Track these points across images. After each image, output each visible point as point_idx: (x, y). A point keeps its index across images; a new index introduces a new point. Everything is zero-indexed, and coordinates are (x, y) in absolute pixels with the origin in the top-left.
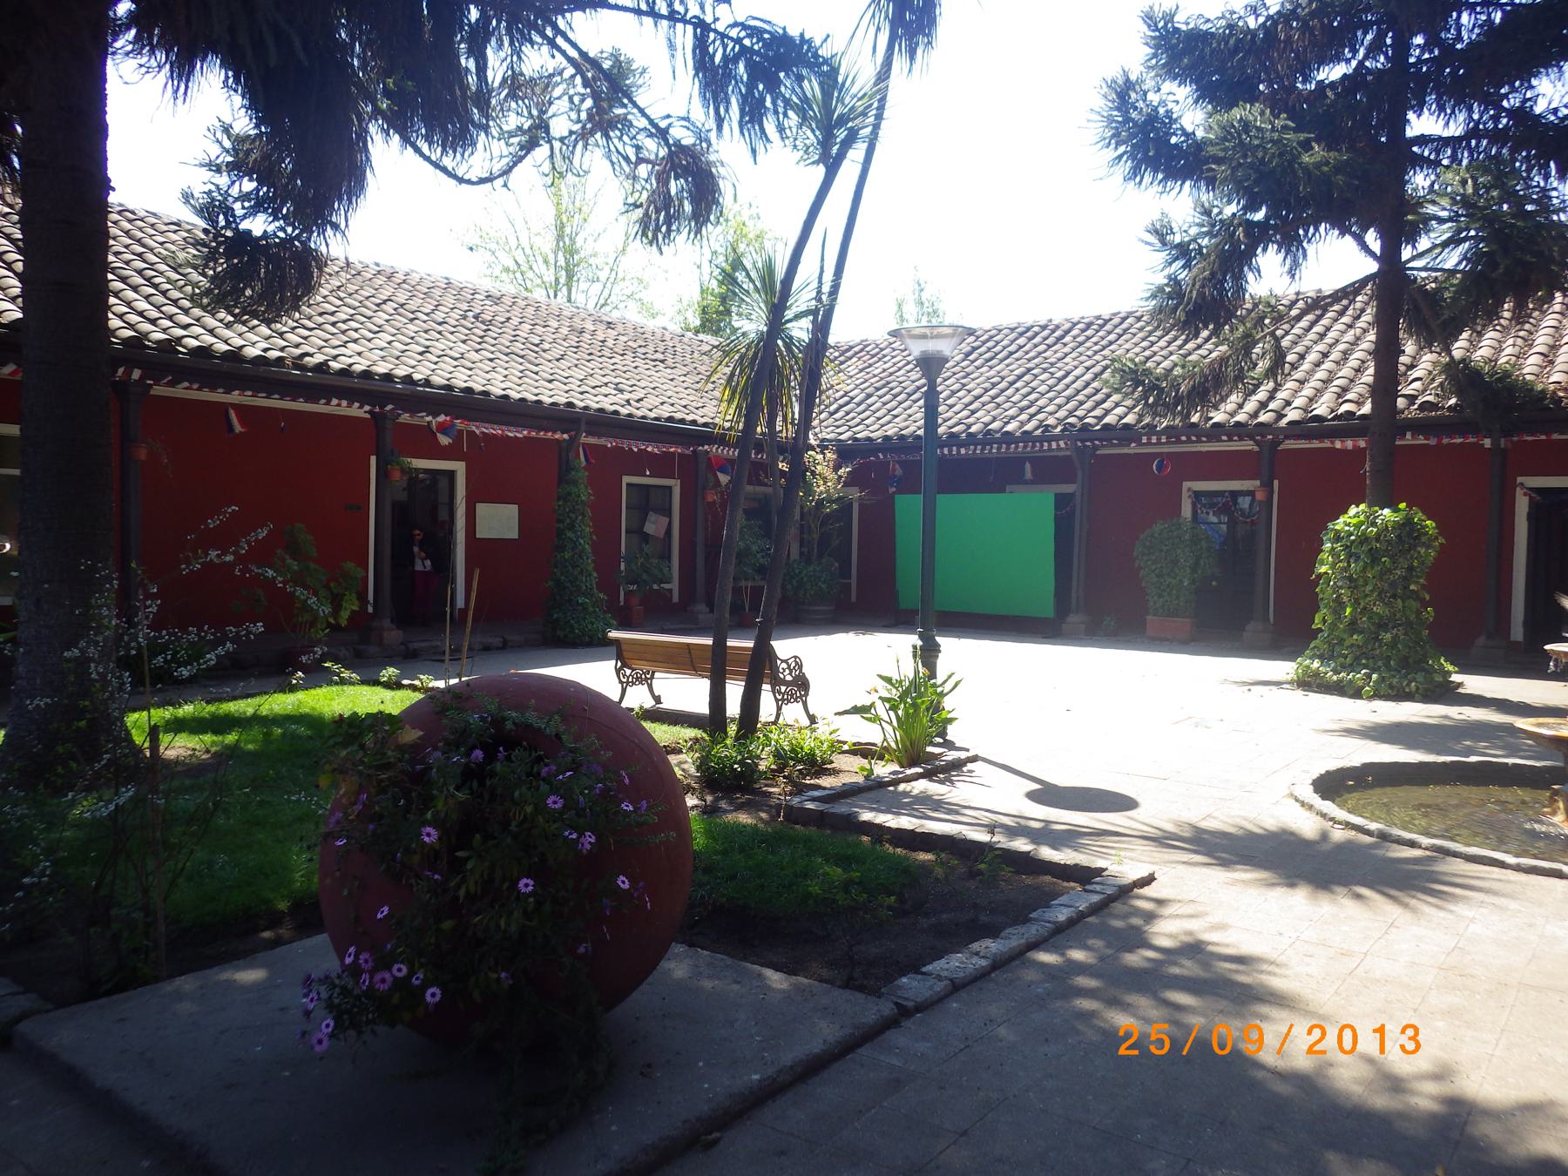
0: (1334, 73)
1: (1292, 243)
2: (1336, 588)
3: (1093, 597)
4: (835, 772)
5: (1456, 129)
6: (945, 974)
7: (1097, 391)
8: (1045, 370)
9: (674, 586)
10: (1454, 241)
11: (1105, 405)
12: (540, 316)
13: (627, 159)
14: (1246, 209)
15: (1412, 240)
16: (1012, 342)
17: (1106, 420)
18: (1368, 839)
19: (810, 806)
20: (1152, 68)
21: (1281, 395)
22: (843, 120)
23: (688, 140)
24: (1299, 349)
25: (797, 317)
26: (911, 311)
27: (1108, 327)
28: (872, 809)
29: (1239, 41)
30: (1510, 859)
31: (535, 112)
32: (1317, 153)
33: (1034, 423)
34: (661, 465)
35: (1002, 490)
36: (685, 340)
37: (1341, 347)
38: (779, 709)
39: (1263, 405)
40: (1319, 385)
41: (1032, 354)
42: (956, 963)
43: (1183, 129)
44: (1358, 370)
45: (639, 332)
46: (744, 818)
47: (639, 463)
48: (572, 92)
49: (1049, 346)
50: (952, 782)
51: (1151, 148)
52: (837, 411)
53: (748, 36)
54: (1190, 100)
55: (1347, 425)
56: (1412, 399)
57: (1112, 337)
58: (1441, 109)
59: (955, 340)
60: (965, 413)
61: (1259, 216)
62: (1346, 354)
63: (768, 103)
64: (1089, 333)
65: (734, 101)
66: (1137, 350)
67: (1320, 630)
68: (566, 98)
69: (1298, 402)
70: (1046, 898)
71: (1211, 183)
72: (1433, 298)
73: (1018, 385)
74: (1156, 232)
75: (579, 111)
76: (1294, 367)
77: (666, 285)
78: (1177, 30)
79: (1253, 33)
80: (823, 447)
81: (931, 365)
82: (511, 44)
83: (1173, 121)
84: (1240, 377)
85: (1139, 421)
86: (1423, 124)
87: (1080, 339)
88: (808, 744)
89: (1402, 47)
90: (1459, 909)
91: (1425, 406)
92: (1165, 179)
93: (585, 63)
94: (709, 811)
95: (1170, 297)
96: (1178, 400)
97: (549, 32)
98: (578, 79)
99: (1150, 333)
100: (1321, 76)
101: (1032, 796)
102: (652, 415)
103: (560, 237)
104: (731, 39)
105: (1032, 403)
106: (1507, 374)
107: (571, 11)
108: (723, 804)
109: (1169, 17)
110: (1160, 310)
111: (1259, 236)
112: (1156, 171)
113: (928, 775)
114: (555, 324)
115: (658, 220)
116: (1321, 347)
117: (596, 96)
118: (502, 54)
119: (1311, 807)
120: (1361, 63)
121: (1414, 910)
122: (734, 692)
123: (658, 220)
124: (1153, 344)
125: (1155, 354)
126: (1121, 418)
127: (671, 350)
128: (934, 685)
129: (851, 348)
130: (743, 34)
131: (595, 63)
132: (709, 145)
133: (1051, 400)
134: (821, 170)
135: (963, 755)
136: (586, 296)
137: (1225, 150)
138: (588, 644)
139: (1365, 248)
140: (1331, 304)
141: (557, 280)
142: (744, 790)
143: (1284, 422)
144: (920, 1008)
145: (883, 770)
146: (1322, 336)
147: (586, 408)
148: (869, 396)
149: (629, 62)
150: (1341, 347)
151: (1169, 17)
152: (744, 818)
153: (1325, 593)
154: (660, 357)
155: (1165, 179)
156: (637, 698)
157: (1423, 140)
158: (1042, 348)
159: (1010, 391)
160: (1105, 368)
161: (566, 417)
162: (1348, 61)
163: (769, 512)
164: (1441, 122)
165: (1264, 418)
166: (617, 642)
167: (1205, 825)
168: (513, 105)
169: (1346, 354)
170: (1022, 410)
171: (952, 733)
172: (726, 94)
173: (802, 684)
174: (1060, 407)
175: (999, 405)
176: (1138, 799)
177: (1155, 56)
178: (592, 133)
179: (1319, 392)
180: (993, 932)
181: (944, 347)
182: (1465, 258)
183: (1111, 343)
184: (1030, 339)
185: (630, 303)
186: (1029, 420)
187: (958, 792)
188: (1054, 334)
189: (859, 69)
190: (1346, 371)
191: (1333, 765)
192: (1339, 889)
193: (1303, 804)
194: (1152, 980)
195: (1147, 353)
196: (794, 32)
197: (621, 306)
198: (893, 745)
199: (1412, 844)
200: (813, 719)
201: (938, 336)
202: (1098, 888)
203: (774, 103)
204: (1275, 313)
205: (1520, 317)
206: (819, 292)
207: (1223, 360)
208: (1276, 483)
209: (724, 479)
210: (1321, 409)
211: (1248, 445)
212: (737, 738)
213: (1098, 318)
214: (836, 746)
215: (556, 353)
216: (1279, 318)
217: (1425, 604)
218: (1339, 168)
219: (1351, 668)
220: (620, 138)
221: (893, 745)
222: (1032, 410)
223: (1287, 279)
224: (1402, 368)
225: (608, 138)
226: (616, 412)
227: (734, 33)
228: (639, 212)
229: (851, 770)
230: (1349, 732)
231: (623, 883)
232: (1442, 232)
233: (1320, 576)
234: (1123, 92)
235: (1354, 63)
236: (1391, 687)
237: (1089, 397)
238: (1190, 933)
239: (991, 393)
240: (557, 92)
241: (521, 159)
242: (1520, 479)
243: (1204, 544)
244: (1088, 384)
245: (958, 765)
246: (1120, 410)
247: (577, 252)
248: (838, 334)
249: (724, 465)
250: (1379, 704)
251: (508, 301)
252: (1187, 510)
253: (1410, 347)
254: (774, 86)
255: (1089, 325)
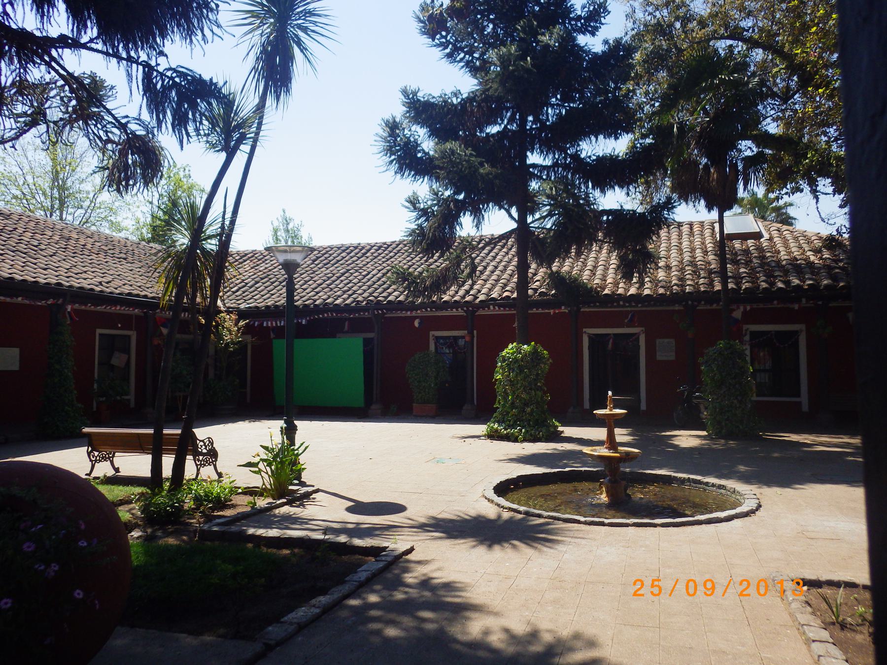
0: (494, 129)
1: (477, 214)
2: (505, 386)
3: (387, 396)
4: (234, 506)
5: (548, 162)
6: (295, 620)
7: (385, 283)
8: (357, 271)
9: (131, 397)
10: (550, 214)
11: (389, 291)
12: (39, 228)
13: (100, 138)
14: (455, 193)
15: (532, 213)
16: (339, 255)
17: (389, 299)
18: (520, 516)
19: (215, 529)
20: (407, 118)
21: (476, 287)
22: (239, 126)
23: (141, 132)
24: (484, 264)
25: (210, 237)
26: (281, 234)
27: (390, 249)
28: (255, 527)
29: (449, 109)
30: (582, 519)
31: (35, 104)
32: (486, 169)
33: (351, 300)
34: (126, 321)
35: (334, 336)
36: (141, 246)
37: (503, 264)
38: (198, 470)
39: (467, 292)
40: (493, 282)
41: (349, 262)
42: (302, 613)
43: (423, 150)
44: (511, 276)
45: (109, 240)
46: (171, 541)
47: (109, 320)
48: (62, 95)
49: (359, 258)
50: (304, 506)
51: (407, 159)
52: (237, 291)
53: (177, 76)
54: (426, 136)
55: (505, 302)
56: (535, 290)
57: (392, 254)
58: (542, 152)
59: (303, 255)
60: (313, 293)
61: (461, 197)
62: (506, 267)
63: (190, 116)
64: (380, 251)
65: (169, 112)
66: (405, 261)
67: (498, 408)
68: (58, 98)
69: (484, 291)
70: (354, 568)
71: (438, 179)
72: (542, 242)
73: (342, 278)
74: (410, 202)
75: (67, 107)
76: (482, 273)
77: (132, 213)
78: (419, 100)
79: (455, 106)
80: (229, 311)
81: (290, 267)
82: (20, 62)
83: (418, 145)
84: (456, 278)
85: (406, 300)
86: (534, 158)
87: (375, 255)
88: (216, 490)
89: (523, 121)
90: (560, 547)
91: (542, 294)
92: (416, 174)
93: (70, 79)
94: (148, 539)
95: (418, 235)
96: (425, 289)
97: (47, 58)
98: (67, 88)
99: (411, 253)
100: (488, 131)
101: (349, 510)
102: (117, 291)
103: (55, 178)
104: (168, 77)
105: (350, 289)
106: (576, 279)
107: (63, 48)
108: (159, 533)
109: (415, 93)
110: (413, 243)
111: (461, 207)
112: (410, 171)
113: (290, 503)
114: (50, 234)
115: (119, 177)
116: (494, 263)
117: (78, 99)
118: (13, 67)
119: (492, 501)
120: (506, 126)
121: (540, 551)
122: (168, 462)
123: (119, 177)
124: (413, 258)
125: (414, 264)
126: (397, 298)
127: (131, 252)
128: (293, 450)
129: (246, 255)
130: (174, 75)
131: (78, 80)
132: (154, 135)
133: (360, 287)
134: (223, 156)
135: (310, 489)
136: (73, 216)
137: (444, 163)
138: (67, 438)
139: (510, 216)
140: (498, 242)
141: (52, 206)
142: (174, 523)
143: (478, 300)
144: (279, 643)
145: (262, 502)
146: (494, 258)
147: (71, 286)
148: (257, 283)
149: (103, 81)
150: (503, 264)
151: (415, 93)
152: (171, 541)
153: (499, 389)
154: (124, 256)
155: (416, 174)
156: (103, 469)
157: (534, 166)
158: (355, 258)
159: (338, 282)
160: (388, 271)
161: (56, 291)
162: (500, 125)
163: (209, 342)
164: (542, 158)
165: (468, 298)
166: (89, 435)
167: (440, 516)
168: (20, 98)
169: (506, 267)
170: (344, 292)
171: (305, 477)
172: (163, 107)
173: (213, 454)
174: (365, 291)
175: (331, 289)
176: (407, 506)
177: (408, 112)
178: (76, 120)
179: (494, 286)
180: (324, 592)
181: (298, 258)
182: (553, 224)
183: (391, 257)
184: (348, 254)
185: (104, 223)
186: (348, 298)
187: (309, 511)
188: (360, 251)
189: (247, 103)
190: (505, 276)
191: (503, 478)
192: (506, 545)
193: (489, 500)
194: (409, 607)
195: (410, 263)
196: (206, 77)
197: (98, 224)
198: (269, 487)
199: (539, 516)
200: (220, 475)
201: (294, 251)
202: (383, 558)
203: (194, 115)
204: (469, 245)
205: (579, 254)
206: (223, 224)
207: (447, 269)
208: (475, 332)
209: (165, 331)
210: (495, 295)
211: (460, 312)
212: (169, 491)
213: (385, 243)
214: (234, 491)
215: (50, 251)
216: (473, 248)
217: (545, 393)
218: (496, 177)
219: (513, 426)
220: (95, 126)
221: (269, 487)
222: (350, 292)
223: (475, 229)
224: (530, 275)
225: (87, 124)
226: (92, 290)
227: (169, 74)
228: (107, 172)
229: (243, 504)
230: (512, 460)
231: (79, 594)
232: (545, 210)
233: (496, 380)
234: (393, 127)
235: (503, 126)
236: (531, 435)
237: (380, 286)
238: (424, 575)
239: (328, 282)
240: (53, 93)
241: (25, 132)
242: (584, 330)
243: (441, 364)
244: (379, 279)
245: (307, 495)
246: (396, 293)
247: (67, 189)
248: (238, 244)
249: (165, 323)
250: (526, 445)
251: (16, 217)
252: (432, 347)
253: (534, 266)
254: (194, 106)
255: (380, 247)
